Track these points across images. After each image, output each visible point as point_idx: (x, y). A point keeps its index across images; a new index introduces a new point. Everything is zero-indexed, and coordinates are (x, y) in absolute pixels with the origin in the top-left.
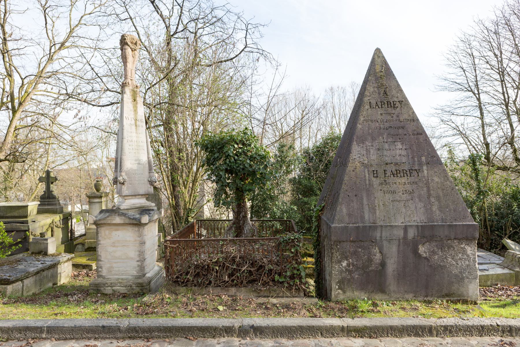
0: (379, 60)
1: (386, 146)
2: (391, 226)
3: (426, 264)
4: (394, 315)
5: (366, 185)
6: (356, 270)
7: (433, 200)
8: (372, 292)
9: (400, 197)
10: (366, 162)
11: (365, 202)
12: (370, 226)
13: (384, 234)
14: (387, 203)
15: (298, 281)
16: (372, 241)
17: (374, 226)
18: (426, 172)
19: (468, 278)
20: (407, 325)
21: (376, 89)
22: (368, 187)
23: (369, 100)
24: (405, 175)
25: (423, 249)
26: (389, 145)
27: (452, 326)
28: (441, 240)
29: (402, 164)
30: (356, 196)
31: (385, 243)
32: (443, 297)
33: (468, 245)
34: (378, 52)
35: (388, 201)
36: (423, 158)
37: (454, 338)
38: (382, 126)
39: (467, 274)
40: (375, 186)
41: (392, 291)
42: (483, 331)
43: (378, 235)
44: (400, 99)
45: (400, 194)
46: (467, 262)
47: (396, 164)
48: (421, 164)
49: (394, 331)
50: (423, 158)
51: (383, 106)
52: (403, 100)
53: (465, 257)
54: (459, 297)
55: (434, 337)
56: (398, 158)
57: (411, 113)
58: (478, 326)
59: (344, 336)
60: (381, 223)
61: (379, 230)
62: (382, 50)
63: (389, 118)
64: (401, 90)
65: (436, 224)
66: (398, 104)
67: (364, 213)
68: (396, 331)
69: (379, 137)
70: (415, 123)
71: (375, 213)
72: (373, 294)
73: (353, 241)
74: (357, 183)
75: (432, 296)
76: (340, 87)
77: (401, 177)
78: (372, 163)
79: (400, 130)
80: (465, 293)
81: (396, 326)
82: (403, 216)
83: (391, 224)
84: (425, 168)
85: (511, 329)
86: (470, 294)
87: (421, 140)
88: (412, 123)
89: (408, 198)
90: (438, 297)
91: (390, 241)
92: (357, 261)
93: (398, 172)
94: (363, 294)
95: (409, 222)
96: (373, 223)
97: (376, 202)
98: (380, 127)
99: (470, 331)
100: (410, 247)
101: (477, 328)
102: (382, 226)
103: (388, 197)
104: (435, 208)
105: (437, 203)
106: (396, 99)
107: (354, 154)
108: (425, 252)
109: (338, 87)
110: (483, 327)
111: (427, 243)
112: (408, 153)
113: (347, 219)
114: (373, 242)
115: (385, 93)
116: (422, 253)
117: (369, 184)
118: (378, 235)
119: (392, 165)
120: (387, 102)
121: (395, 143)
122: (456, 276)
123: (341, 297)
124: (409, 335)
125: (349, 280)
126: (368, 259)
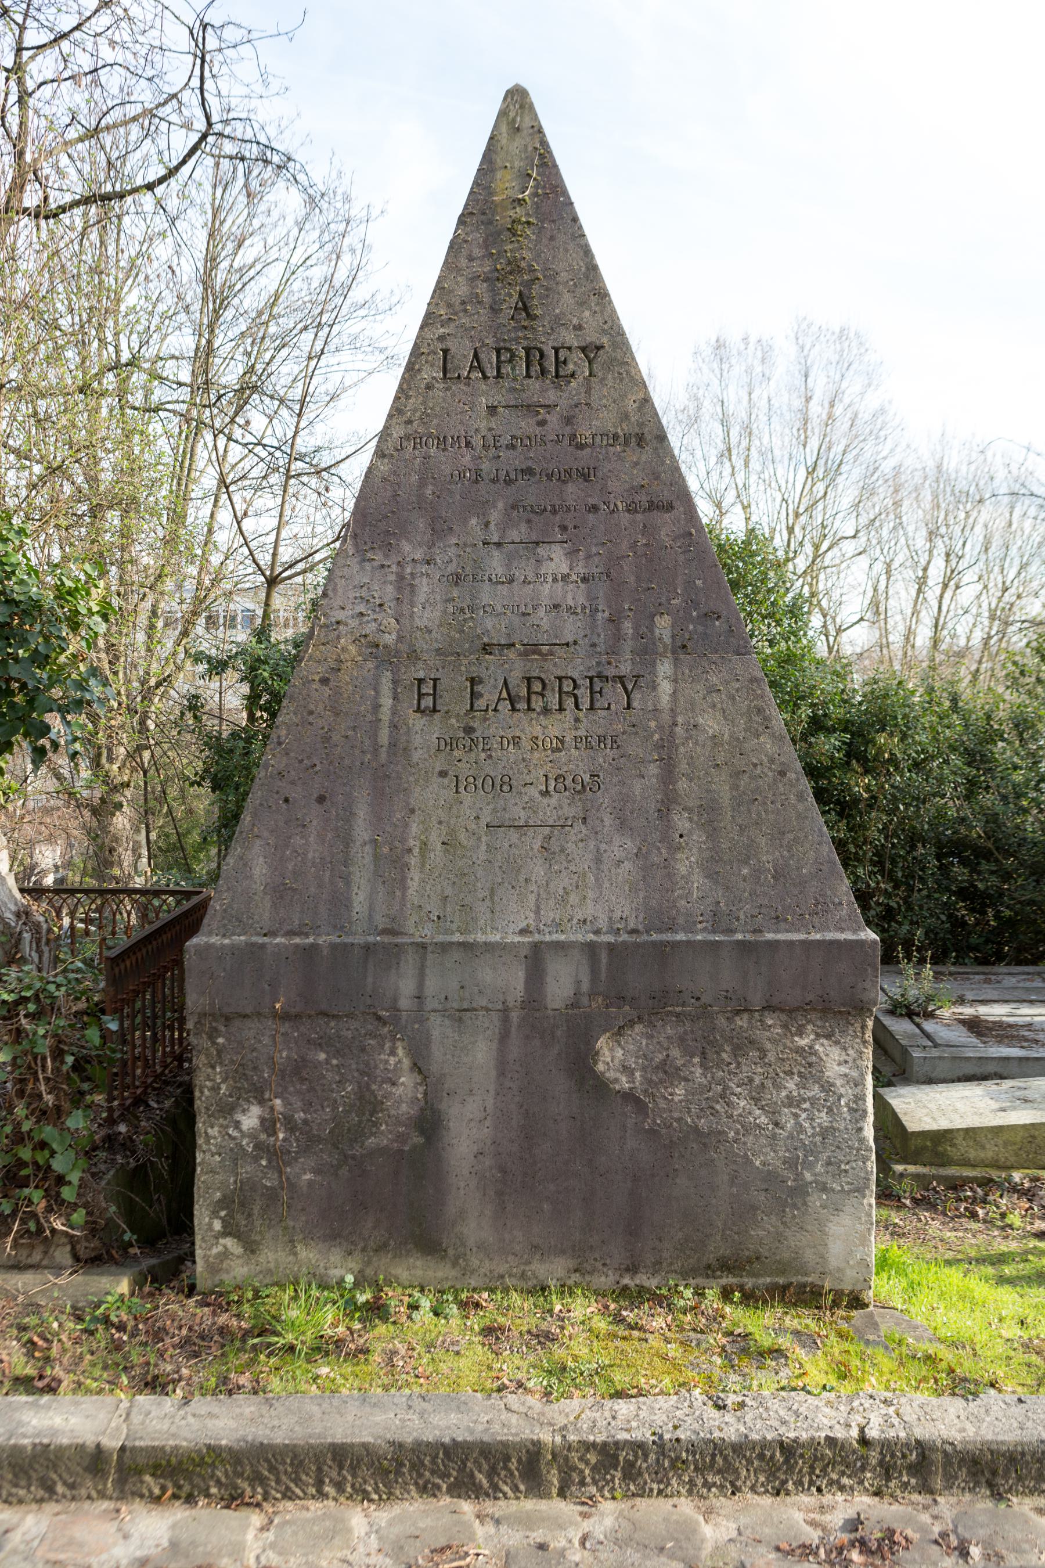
0: (518, 142)
1: (496, 563)
2: (464, 946)
3: (630, 1123)
4: (445, 1368)
5: (376, 748)
6: (305, 1150)
7: (682, 822)
8: (381, 1248)
9: (530, 807)
10: (389, 639)
11: (361, 831)
12: (367, 948)
13: (432, 984)
14: (462, 836)
15: (37, 1195)
16: (379, 1018)
17: (384, 946)
18: (665, 687)
19: (824, 1188)
20: (418, 1444)
21: (482, 288)
22: (383, 756)
23: (442, 338)
24: (569, 702)
25: (619, 1053)
26: (510, 558)
27: (639, 1446)
28: (704, 1012)
29: (560, 652)
30: (321, 799)
31: (438, 1028)
32: (709, 1271)
33: (828, 1037)
34: (517, 100)
35: (472, 826)
36: (663, 625)
37: (641, 1503)
38: (485, 466)
39: (819, 1168)
40: (416, 756)
41: (471, 1242)
42: (791, 1469)
43: (406, 987)
44: (591, 336)
45: (534, 792)
46: (823, 1118)
47: (532, 649)
48: (647, 653)
49: (354, 1469)
50: (663, 625)
51: (506, 369)
52: (605, 340)
53: (815, 1091)
54: (783, 1272)
55: (548, 1496)
56: (545, 624)
57: (631, 406)
58: (764, 1444)
59: (103, 1495)
60: (427, 933)
61: (409, 964)
62: (535, 98)
63: (526, 425)
64: (602, 295)
65: (681, 937)
66: (576, 362)
67: (348, 883)
68: (364, 1471)
69: (465, 521)
70: (646, 455)
71: (403, 883)
72: (383, 1261)
73: (284, 1016)
74: (336, 738)
75: (656, 1268)
76: (753, 340)
77: (546, 711)
78: (421, 645)
79: (570, 488)
80: (809, 1255)
81: (365, 1446)
82: (532, 898)
83: (470, 938)
84: (665, 668)
85: (923, 1456)
86: (833, 1262)
87: (664, 535)
88: (632, 455)
89: (569, 811)
90: (686, 1274)
91: (460, 1016)
92: (307, 1107)
93: (537, 687)
94: (336, 1256)
95: (558, 926)
96: (385, 932)
97: (414, 829)
98: (478, 473)
99: (728, 1470)
100: (554, 1043)
101: (761, 1457)
102: (423, 946)
103: (474, 805)
104: (686, 863)
105: (698, 837)
106: (569, 338)
107: (338, 602)
108: (626, 1069)
109: (745, 340)
110: (789, 1449)
111: (639, 1028)
112: (591, 597)
113: (264, 911)
114: (385, 1019)
115: (524, 307)
116: (611, 1075)
117: (393, 745)
118: (406, 987)
119: (512, 654)
120: (528, 350)
121: (542, 551)
122: (771, 1178)
123: (239, 1270)
124: (427, 1490)
125: (272, 1196)
126: (361, 1098)
